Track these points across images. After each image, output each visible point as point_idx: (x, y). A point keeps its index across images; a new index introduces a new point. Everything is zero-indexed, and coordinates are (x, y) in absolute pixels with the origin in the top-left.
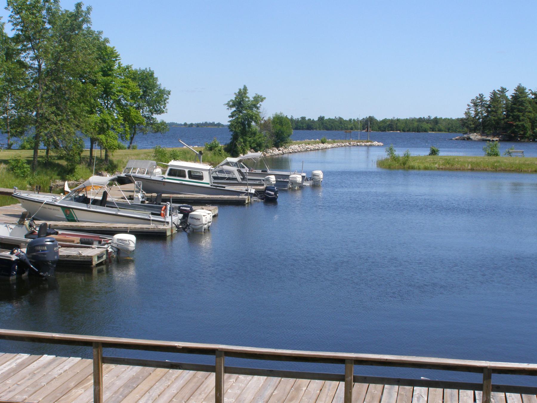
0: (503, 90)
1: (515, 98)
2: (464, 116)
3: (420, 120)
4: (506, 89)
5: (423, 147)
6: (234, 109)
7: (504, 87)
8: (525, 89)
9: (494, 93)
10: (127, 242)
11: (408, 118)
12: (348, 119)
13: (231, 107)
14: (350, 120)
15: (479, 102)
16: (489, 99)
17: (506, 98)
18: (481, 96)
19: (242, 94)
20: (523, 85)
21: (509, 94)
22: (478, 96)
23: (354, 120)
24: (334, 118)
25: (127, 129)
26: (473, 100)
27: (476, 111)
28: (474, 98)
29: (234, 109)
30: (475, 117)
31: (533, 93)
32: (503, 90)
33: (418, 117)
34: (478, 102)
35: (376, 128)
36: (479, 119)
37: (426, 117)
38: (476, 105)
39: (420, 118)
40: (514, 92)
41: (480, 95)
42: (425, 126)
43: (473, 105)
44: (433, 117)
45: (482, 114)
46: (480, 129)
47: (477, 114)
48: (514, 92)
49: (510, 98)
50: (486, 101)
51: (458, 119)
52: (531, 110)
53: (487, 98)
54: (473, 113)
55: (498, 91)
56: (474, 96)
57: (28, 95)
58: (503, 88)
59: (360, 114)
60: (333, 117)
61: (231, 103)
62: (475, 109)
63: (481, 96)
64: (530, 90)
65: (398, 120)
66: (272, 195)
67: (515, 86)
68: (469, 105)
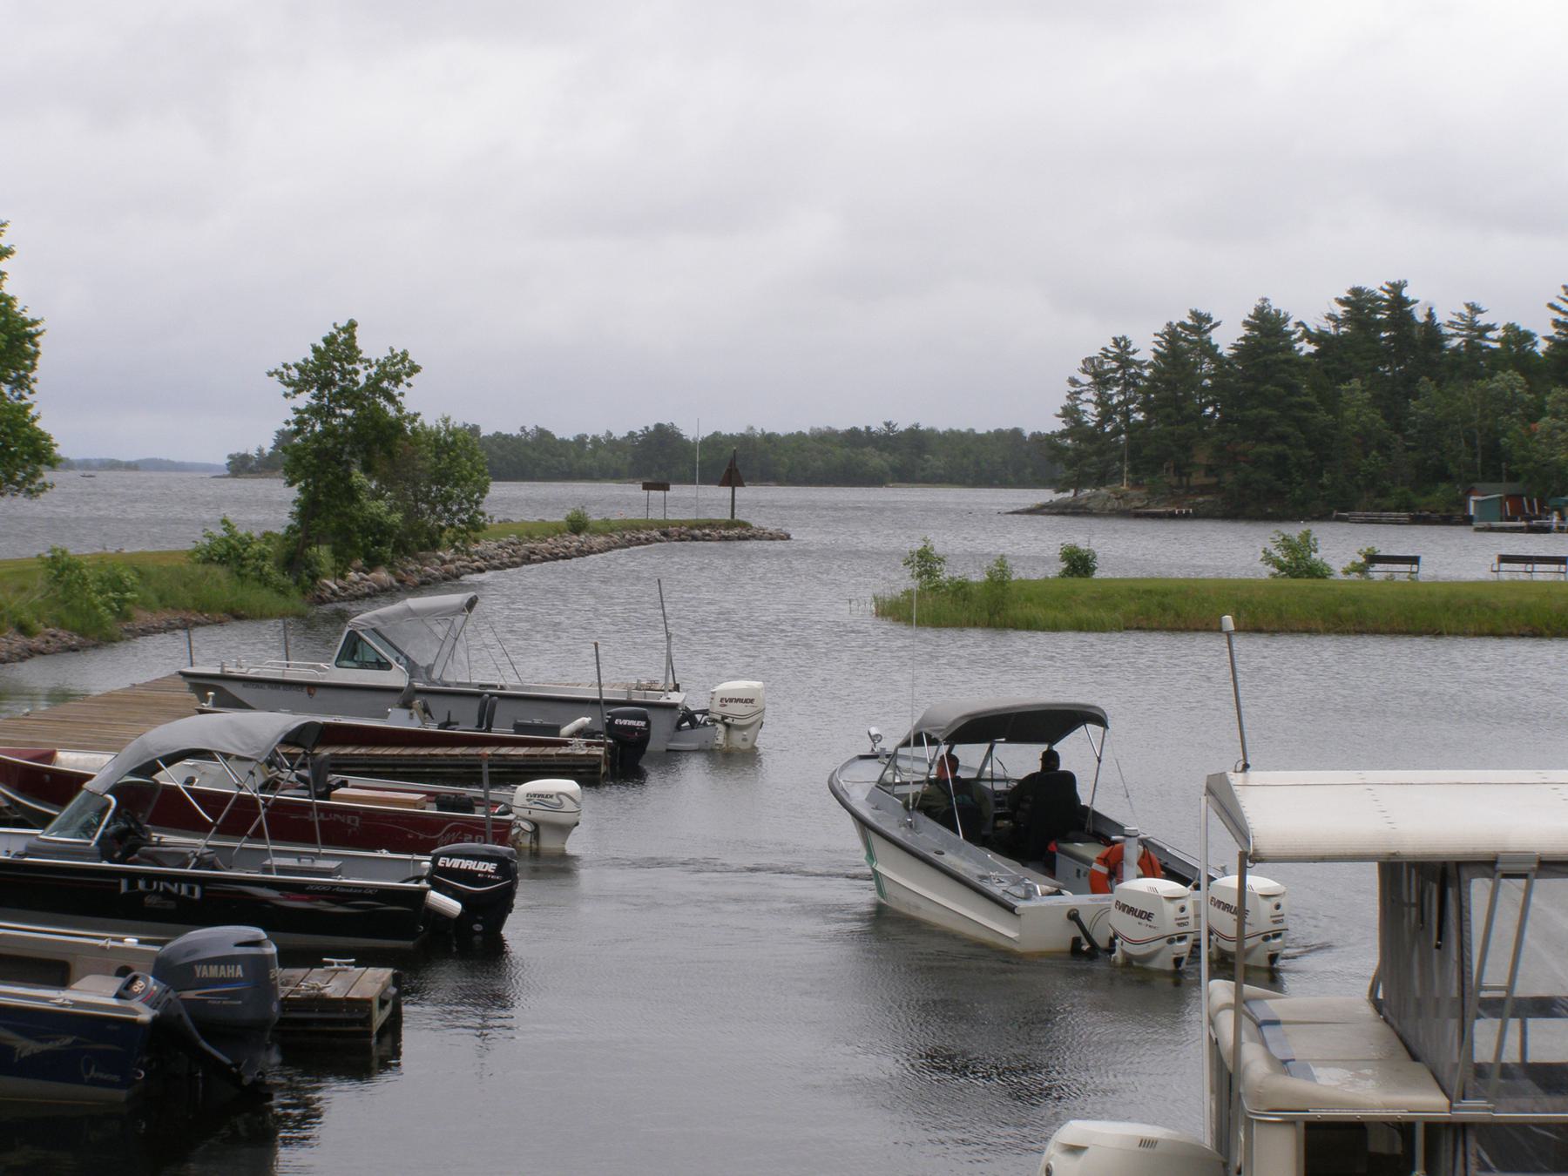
0: (1201, 322)
1: (1246, 351)
3: (854, 437)
4: (1209, 319)
5: (1340, 519)
6: (305, 399)
7: (1203, 311)
8: (1286, 320)
9: (1172, 336)
10: (555, 800)
11: (806, 431)
12: (570, 436)
13: (299, 387)
14: (581, 440)
15: (1114, 371)
16: (1150, 357)
17: (1210, 351)
18: (1122, 344)
19: (339, 348)
20: (1277, 304)
21: (1227, 337)
22: (1109, 344)
23: (596, 440)
24: (516, 432)
25: (1479, 461)
26: (1091, 360)
27: (1102, 403)
28: (1095, 352)
29: (305, 399)
30: (1100, 424)
33: (842, 426)
36: (1117, 432)
37: (877, 426)
38: (1102, 380)
39: (854, 433)
40: (1244, 332)
41: (1116, 342)
42: (876, 460)
43: (1088, 379)
44: (902, 426)
45: (1127, 415)
46: (1120, 472)
47: (1106, 416)
48: (1244, 332)
49: (1225, 350)
50: (1139, 364)
52: (1312, 399)
53: (1145, 349)
54: (1090, 414)
55: (1182, 325)
56: (1096, 341)
57: (1134, 450)
58: (1196, 315)
59: (624, 419)
62: (1100, 397)
63: (1122, 344)
64: (1300, 324)
65: (770, 438)
68: (1073, 382)
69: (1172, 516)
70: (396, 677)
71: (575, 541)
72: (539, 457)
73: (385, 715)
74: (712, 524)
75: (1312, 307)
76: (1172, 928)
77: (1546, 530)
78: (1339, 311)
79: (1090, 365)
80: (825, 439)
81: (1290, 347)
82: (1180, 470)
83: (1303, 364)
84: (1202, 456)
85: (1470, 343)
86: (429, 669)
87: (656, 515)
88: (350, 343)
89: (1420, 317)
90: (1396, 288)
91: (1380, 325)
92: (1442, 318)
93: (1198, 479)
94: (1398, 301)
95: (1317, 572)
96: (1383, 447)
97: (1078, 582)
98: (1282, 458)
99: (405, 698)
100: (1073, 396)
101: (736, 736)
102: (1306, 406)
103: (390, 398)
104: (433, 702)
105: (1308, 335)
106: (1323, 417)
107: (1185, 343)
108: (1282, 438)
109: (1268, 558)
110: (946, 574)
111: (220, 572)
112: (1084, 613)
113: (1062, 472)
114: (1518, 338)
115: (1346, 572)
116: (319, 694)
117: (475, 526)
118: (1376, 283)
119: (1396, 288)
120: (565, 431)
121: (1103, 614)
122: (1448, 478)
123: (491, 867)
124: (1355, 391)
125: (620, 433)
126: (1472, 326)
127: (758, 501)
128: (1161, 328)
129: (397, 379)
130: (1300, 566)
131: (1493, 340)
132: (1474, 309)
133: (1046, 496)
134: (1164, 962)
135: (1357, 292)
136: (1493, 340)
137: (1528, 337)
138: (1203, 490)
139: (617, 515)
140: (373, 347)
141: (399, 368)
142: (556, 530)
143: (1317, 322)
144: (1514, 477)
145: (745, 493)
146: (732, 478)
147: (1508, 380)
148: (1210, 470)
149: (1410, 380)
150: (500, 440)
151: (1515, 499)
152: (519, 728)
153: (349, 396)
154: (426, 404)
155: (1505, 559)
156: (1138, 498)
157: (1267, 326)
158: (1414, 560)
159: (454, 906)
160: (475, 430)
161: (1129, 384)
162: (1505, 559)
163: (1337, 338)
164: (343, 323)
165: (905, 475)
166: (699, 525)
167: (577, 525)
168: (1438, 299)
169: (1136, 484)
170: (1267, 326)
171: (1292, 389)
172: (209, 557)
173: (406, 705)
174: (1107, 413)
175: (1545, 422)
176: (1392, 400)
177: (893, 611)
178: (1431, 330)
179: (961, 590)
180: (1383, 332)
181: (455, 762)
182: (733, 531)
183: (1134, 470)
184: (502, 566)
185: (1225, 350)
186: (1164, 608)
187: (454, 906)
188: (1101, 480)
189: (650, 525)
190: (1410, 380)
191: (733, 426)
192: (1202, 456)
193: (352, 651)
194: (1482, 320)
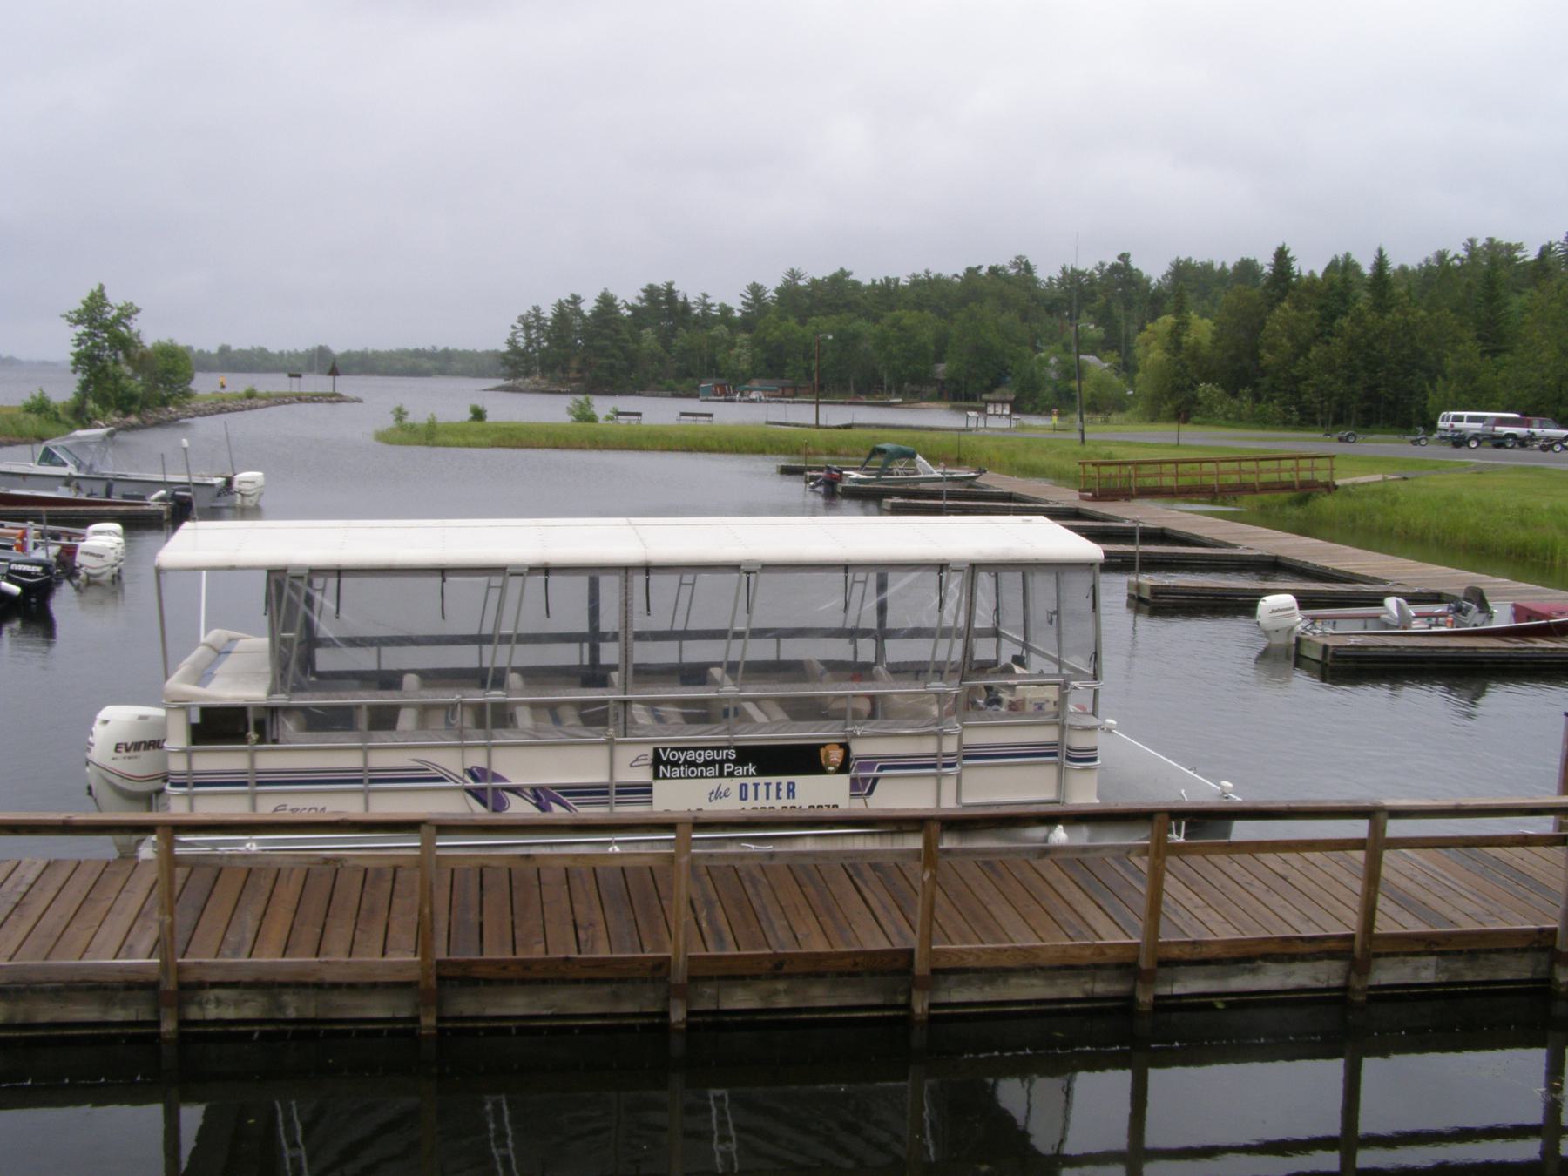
0: (576, 300)
1: (597, 314)
2: (505, 348)
6: (81, 329)
9: (560, 305)
13: (79, 322)
14: (281, 353)
17: (580, 313)
19: (96, 302)
20: (611, 291)
21: (588, 307)
27: (528, 337)
28: (524, 313)
29: (81, 329)
31: (627, 306)
32: (576, 300)
33: (411, 347)
34: (531, 322)
35: (716, 672)
37: (428, 347)
38: (527, 327)
42: (428, 365)
44: (440, 348)
47: (529, 344)
49: (587, 313)
51: (487, 353)
53: (548, 313)
54: (522, 342)
56: (525, 309)
57: (542, 362)
58: (573, 296)
60: (247, 347)
61: (75, 316)
65: (376, 354)
66: (35, 576)
67: (598, 293)
69: (559, 393)
70: (70, 470)
71: (248, 403)
72: (229, 361)
73: (55, 490)
74: (323, 395)
75: (628, 294)
76: (113, 561)
77: (733, 401)
78: (642, 295)
79: (522, 319)
80: (403, 354)
81: (618, 312)
82: (564, 370)
83: (623, 321)
84: (574, 364)
85: (703, 312)
86: (91, 467)
87: (295, 390)
88: (103, 296)
89: (680, 299)
90: (670, 285)
91: (661, 303)
92: (690, 299)
93: (573, 374)
94: (670, 292)
95: (592, 419)
96: (661, 360)
97: (477, 425)
98: (612, 366)
99: (68, 481)
100: (513, 334)
101: (247, 500)
102: (626, 341)
103: (126, 326)
104: (83, 484)
105: (627, 306)
106: (632, 346)
107: (567, 311)
108: (613, 356)
109: (570, 411)
110: (409, 420)
111: (33, 417)
112: (471, 439)
113: (507, 369)
114: (726, 310)
115: (608, 418)
116: (29, 479)
117: (188, 394)
118: (660, 282)
119: (670, 285)
120: (274, 349)
121: (482, 440)
122: (691, 375)
123: (39, 569)
124: (648, 334)
125: (301, 350)
126: (704, 304)
127: (345, 385)
128: (555, 301)
129: (128, 317)
130: (586, 417)
131: (715, 311)
132: (706, 296)
133: (501, 382)
134: (107, 577)
135: (651, 286)
136: (715, 311)
137: (730, 310)
138: (575, 380)
139: (273, 390)
140: (116, 298)
141: (128, 312)
142: (240, 397)
143: (632, 300)
144: (719, 376)
145: (340, 380)
146: (334, 372)
147: (720, 330)
148: (579, 371)
149: (674, 329)
150: (242, 353)
151: (722, 386)
152: (125, 497)
153: (106, 327)
154: (150, 332)
155: (683, 414)
156: (544, 384)
157: (607, 302)
158: (639, 414)
159: (16, 590)
160: (190, 348)
161: (540, 328)
162: (683, 414)
163: (642, 309)
164: (96, 288)
165: (442, 372)
166: (317, 395)
167: (251, 395)
168: (689, 290)
169: (543, 377)
170: (607, 302)
171: (617, 332)
172: (29, 409)
173: (67, 484)
174: (530, 342)
175: (737, 351)
176: (666, 338)
177: (384, 438)
178: (686, 307)
179: (412, 429)
180: (663, 306)
181: (64, 514)
182: (334, 398)
183: (542, 370)
184: (205, 415)
185: (587, 313)
186: (511, 437)
187: (16, 590)
188: (527, 374)
189: (290, 395)
190: (674, 329)
191: (357, 347)
192: (574, 364)
193: (48, 457)
194: (709, 301)
